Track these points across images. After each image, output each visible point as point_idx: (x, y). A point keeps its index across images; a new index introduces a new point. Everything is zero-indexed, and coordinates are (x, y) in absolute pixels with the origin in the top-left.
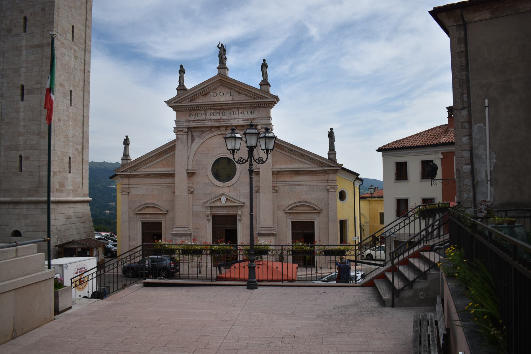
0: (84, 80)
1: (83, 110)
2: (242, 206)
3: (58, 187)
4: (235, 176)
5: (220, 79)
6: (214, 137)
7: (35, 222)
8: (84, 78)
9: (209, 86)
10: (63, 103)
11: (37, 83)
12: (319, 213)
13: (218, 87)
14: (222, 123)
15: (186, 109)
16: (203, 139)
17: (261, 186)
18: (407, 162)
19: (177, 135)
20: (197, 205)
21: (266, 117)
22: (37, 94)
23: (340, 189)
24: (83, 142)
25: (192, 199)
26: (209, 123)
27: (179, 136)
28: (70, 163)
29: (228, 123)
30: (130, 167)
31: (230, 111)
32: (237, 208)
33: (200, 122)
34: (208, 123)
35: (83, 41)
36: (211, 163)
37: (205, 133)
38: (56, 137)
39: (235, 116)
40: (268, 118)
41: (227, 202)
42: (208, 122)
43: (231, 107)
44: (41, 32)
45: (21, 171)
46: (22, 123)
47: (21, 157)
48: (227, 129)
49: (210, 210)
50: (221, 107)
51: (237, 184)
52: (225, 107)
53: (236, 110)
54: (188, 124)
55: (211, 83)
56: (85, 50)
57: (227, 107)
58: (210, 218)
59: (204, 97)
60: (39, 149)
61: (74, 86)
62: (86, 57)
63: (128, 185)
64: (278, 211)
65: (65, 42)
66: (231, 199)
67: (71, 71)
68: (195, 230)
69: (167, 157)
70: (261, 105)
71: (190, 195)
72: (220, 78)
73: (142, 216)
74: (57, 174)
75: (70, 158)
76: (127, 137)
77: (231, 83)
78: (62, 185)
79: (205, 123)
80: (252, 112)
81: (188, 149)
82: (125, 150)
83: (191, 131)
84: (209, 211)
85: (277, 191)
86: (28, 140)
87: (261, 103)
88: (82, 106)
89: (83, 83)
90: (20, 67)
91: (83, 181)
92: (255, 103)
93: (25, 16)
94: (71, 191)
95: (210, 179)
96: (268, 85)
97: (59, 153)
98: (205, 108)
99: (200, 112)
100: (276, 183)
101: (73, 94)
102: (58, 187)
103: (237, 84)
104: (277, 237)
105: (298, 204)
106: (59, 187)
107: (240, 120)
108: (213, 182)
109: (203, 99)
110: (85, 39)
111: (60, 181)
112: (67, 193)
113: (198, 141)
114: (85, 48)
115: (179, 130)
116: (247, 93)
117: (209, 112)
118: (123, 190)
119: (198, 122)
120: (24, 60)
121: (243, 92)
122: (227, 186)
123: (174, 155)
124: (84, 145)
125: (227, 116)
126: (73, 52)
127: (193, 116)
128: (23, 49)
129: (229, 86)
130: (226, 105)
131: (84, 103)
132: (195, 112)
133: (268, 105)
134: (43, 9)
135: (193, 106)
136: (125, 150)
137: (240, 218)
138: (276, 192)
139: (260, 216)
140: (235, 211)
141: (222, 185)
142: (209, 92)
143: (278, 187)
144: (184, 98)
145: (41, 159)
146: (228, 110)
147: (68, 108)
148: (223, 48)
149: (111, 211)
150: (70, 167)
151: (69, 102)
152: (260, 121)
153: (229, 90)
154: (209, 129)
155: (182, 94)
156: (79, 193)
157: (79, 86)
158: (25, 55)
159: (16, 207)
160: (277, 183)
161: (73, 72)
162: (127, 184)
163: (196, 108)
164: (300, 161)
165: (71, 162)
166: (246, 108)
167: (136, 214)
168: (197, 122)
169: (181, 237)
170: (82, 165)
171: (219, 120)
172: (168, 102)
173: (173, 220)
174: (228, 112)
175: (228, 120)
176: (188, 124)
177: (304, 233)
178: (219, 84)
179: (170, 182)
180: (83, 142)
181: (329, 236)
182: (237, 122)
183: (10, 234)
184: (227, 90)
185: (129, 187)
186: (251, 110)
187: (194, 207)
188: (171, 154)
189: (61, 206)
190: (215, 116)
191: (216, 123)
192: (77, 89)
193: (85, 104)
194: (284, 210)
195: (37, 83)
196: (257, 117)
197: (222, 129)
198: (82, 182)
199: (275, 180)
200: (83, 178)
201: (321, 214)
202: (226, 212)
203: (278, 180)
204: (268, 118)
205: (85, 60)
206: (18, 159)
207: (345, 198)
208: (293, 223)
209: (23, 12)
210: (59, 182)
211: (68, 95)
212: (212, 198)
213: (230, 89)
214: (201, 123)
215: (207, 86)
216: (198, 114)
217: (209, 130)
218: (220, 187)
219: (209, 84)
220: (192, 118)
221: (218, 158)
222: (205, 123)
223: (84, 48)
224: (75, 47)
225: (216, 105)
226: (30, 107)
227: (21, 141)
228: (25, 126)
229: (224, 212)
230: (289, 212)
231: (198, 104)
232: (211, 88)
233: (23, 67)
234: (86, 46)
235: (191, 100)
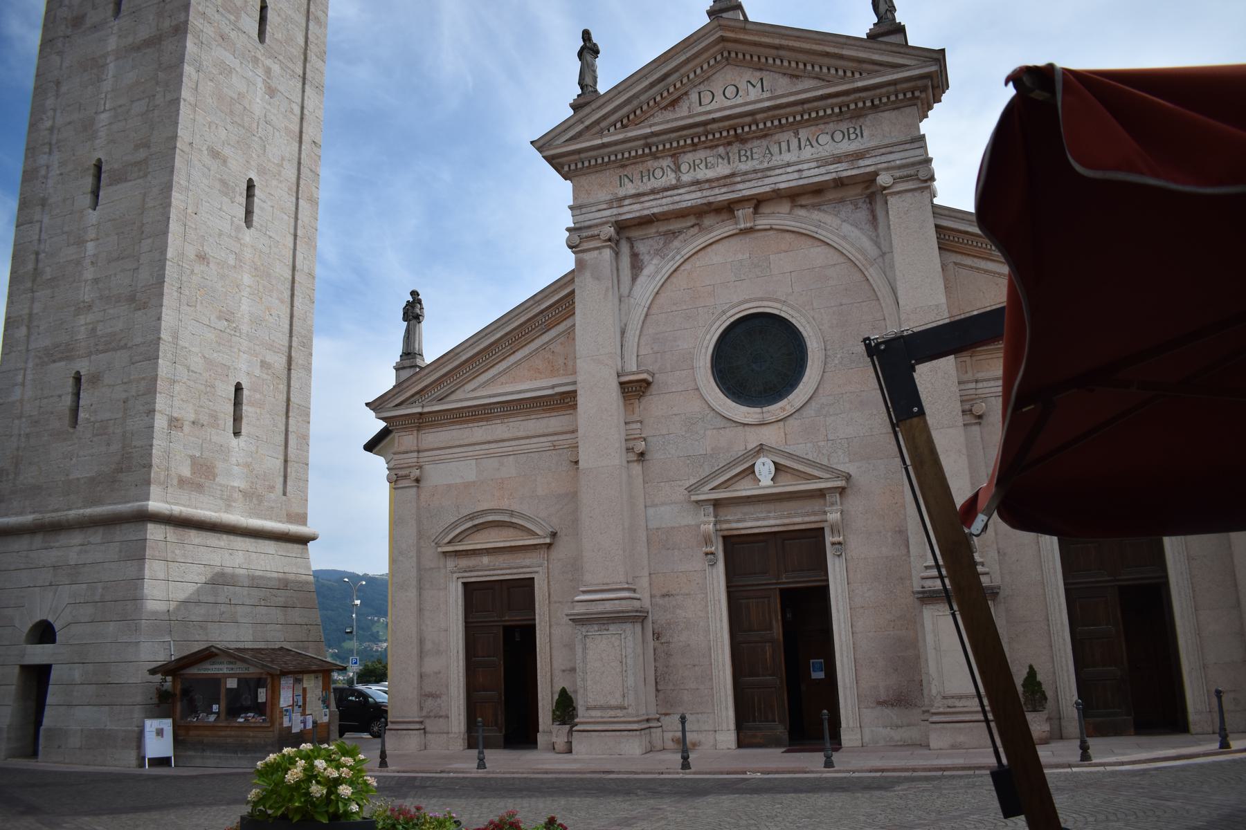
0: (299, 163)
2: (842, 491)
3: (186, 472)
4: (805, 379)
6: (714, 247)
7: (100, 590)
8: (300, 159)
9: (683, 71)
10: (220, 209)
13: (714, 71)
14: (740, 186)
15: (606, 159)
16: (673, 258)
19: (581, 255)
20: (663, 504)
21: (909, 138)
22: (135, 180)
24: (290, 347)
25: (644, 482)
26: (693, 196)
27: (586, 256)
28: (237, 403)
29: (760, 184)
30: (422, 390)
31: (764, 142)
32: (822, 502)
33: (658, 196)
34: (687, 197)
35: (297, 52)
36: (706, 342)
37: (680, 238)
38: (184, 308)
39: (787, 157)
40: (913, 141)
41: (779, 479)
46: (89, 274)
49: (716, 516)
52: (746, 129)
54: (615, 211)
55: (688, 55)
56: (304, 79)
57: (754, 128)
58: (717, 548)
60: (129, 345)
62: (306, 98)
63: (415, 455)
65: (233, 35)
67: (255, 125)
68: (660, 601)
69: (547, 343)
71: (637, 468)
73: (464, 562)
74: (187, 428)
75: (238, 388)
76: (414, 294)
79: (677, 198)
80: (851, 130)
81: (620, 301)
82: (408, 338)
83: (628, 239)
84: (712, 519)
85: (980, 417)
86: (102, 321)
87: (884, 90)
88: (291, 239)
89: (296, 172)
91: (289, 470)
92: (857, 95)
94: (236, 495)
95: (709, 399)
99: (656, 164)
100: (973, 385)
101: (257, 192)
102: (186, 472)
103: (784, 42)
106: (193, 473)
107: (805, 166)
110: (306, 49)
111: (198, 454)
112: (222, 499)
113: (655, 270)
114: (304, 74)
115: (587, 237)
117: (689, 157)
118: (401, 473)
119: (652, 197)
120: (109, 89)
122: (773, 419)
124: (293, 354)
125: (755, 162)
126: (260, 71)
127: (632, 181)
130: (748, 119)
132: (640, 167)
136: (408, 338)
137: (836, 539)
138: (980, 424)
140: (814, 513)
141: (757, 416)
142: (686, 93)
145: (132, 377)
146: (758, 142)
150: (237, 419)
151: (241, 213)
152: (884, 158)
153: (758, 74)
156: (272, 508)
158: (113, 77)
159: (52, 544)
160: (980, 385)
161: (260, 129)
162: (412, 452)
165: (245, 401)
166: (825, 119)
167: (444, 553)
168: (646, 198)
169: (606, 626)
170: (284, 420)
171: (728, 181)
172: (540, 143)
173: (575, 566)
174: (758, 147)
175: (759, 175)
176: (615, 211)
177: (1118, 583)
178: (719, 58)
179: (559, 429)
180: (290, 347)
181: (1236, 585)
182: (796, 175)
183: (25, 635)
185: (421, 460)
186: (844, 126)
187: (651, 511)
188: (562, 327)
189: (194, 536)
190: (713, 166)
191: (717, 191)
192: (275, 183)
193: (299, 233)
195: (137, 147)
196: (873, 144)
197: (740, 213)
198: (282, 474)
199: (969, 376)
202: (778, 522)
203: (980, 376)
204: (913, 141)
210: (192, 458)
211: (237, 189)
213: (761, 69)
214: (664, 201)
215: (676, 69)
216: (651, 174)
217: (692, 226)
218: (747, 428)
219: (683, 58)
221: (732, 320)
222: (677, 198)
223: (301, 73)
224: (268, 62)
226: (114, 220)
227: (83, 328)
229: (772, 522)
233: (105, 110)
234: (307, 70)
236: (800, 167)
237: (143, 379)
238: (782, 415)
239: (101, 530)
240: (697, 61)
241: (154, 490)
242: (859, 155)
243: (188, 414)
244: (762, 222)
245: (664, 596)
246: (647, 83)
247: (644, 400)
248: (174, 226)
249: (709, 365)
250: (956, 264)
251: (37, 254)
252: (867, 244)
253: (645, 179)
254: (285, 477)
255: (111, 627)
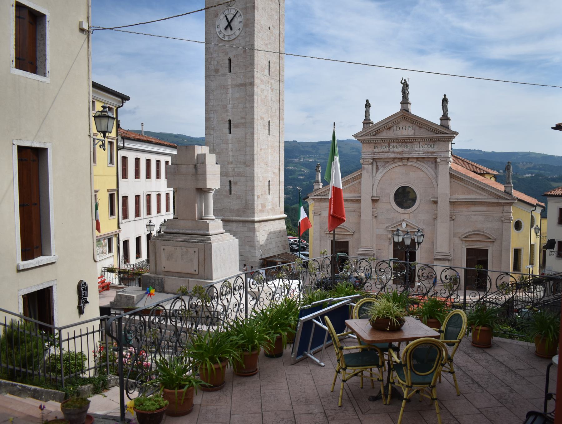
0: (279, 109)
1: (279, 136)
4: (415, 204)
5: (403, 115)
8: (279, 107)
11: (242, 118)
12: (493, 242)
14: (404, 155)
16: (387, 169)
17: (439, 215)
18: (515, 249)
20: (380, 229)
23: (514, 219)
24: (279, 166)
25: (376, 223)
26: (393, 155)
28: (269, 185)
31: (411, 144)
38: (259, 165)
39: (416, 149)
41: (407, 227)
42: (391, 154)
43: (413, 140)
44: (244, 72)
45: (231, 193)
46: (231, 153)
47: (230, 182)
48: (409, 160)
50: (403, 141)
51: (417, 210)
52: (407, 140)
53: (417, 143)
54: (373, 155)
56: (280, 80)
57: (409, 140)
59: (388, 131)
60: (245, 176)
61: (271, 117)
64: (454, 238)
66: (411, 225)
68: (378, 251)
70: (441, 140)
71: (374, 220)
72: (402, 114)
75: (269, 181)
77: (413, 118)
78: (264, 206)
79: (389, 155)
83: (376, 161)
85: (454, 219)
90: (227, 104)
93: (230, 58)
94: (270, 211)
96: (448, 119)
97: (261, 179)
98: (389, 141)
99: (384, 144)
101: (271, 124)
104: (452, 261)
105: (473, 233)
106: (262, 208)
107: (420, 153)
108: (395, 208)
109: (387, 133)
110: (280, 70)
113: (382, 171)
114: (280, 79)
116: (428, 128)
117: (392, 144)
118: (315, 212)
121: (424, 127)
123: (360, 183)
125: (408, 149)
126: (270, 86)
128: (229, 87)
129: (411, 121)
130: (408, 139)
131: (279, 130)
132: (380, 144)
133: (447, 139)
134: (245, 51)
135: (377, 139)
139: (437, 242)
142: (393, 126)
143: (455, 216)
144: (370, 132)
147: (267, 137)
148: (406, 83)
149: (288, 196)
150: (269, 190)
152: (440, 154)
153: (411, 124)
154: (392, 160)
155: (367, 129)
157: (275, 115)
163: (380, 141)
164: (476, 192)
166: (427, 141)
167: (327, 233)
173: (359, 240)
174: (410, 145)
175: (409, 153)
176: (373, 155)
178: (402, 119)
180: (279, 166)
182: (418, 155)
184: (409, 124)
186: (431, 144)
187: (377, 230)
189: (263, 223)
191: (398, 155)
194: (460, 238)
197: (404, 160)
200: (279, 198)
201: (495, 244)
205: (280, 90)
206: (228, 184)
207: (521, 228)
208: (468, 250)
209: (227, 54)
210: (261, 204)
212: (393, 223)
213: (412, 123)
214: (385, 155)
216: (382, 147)
220: (377, 150)
222: (389, 155)
225: (399, 139)
228: (233, 156)
230: (466, 238)
231: (382, 138)
232: (394, 122)
233: (230, 104)
235: (376, 133)
236: (419, 153)
237: (250, 186)
238: (409, 212)
239: (242, 223)
240: (396, 119)
241: (256, 215)
242: (434, 153)
243: (260, 194)
244: (409, 163)
245: (379, 250)
246: (383, 124)
247: (377, 203)
248: (255, 145)
249: (393, 197)
250: (453, 181)
251: (213, 144)
252: (433, 173)
253: (381, 148)
254: (279, 202)
255: (247, 248)
